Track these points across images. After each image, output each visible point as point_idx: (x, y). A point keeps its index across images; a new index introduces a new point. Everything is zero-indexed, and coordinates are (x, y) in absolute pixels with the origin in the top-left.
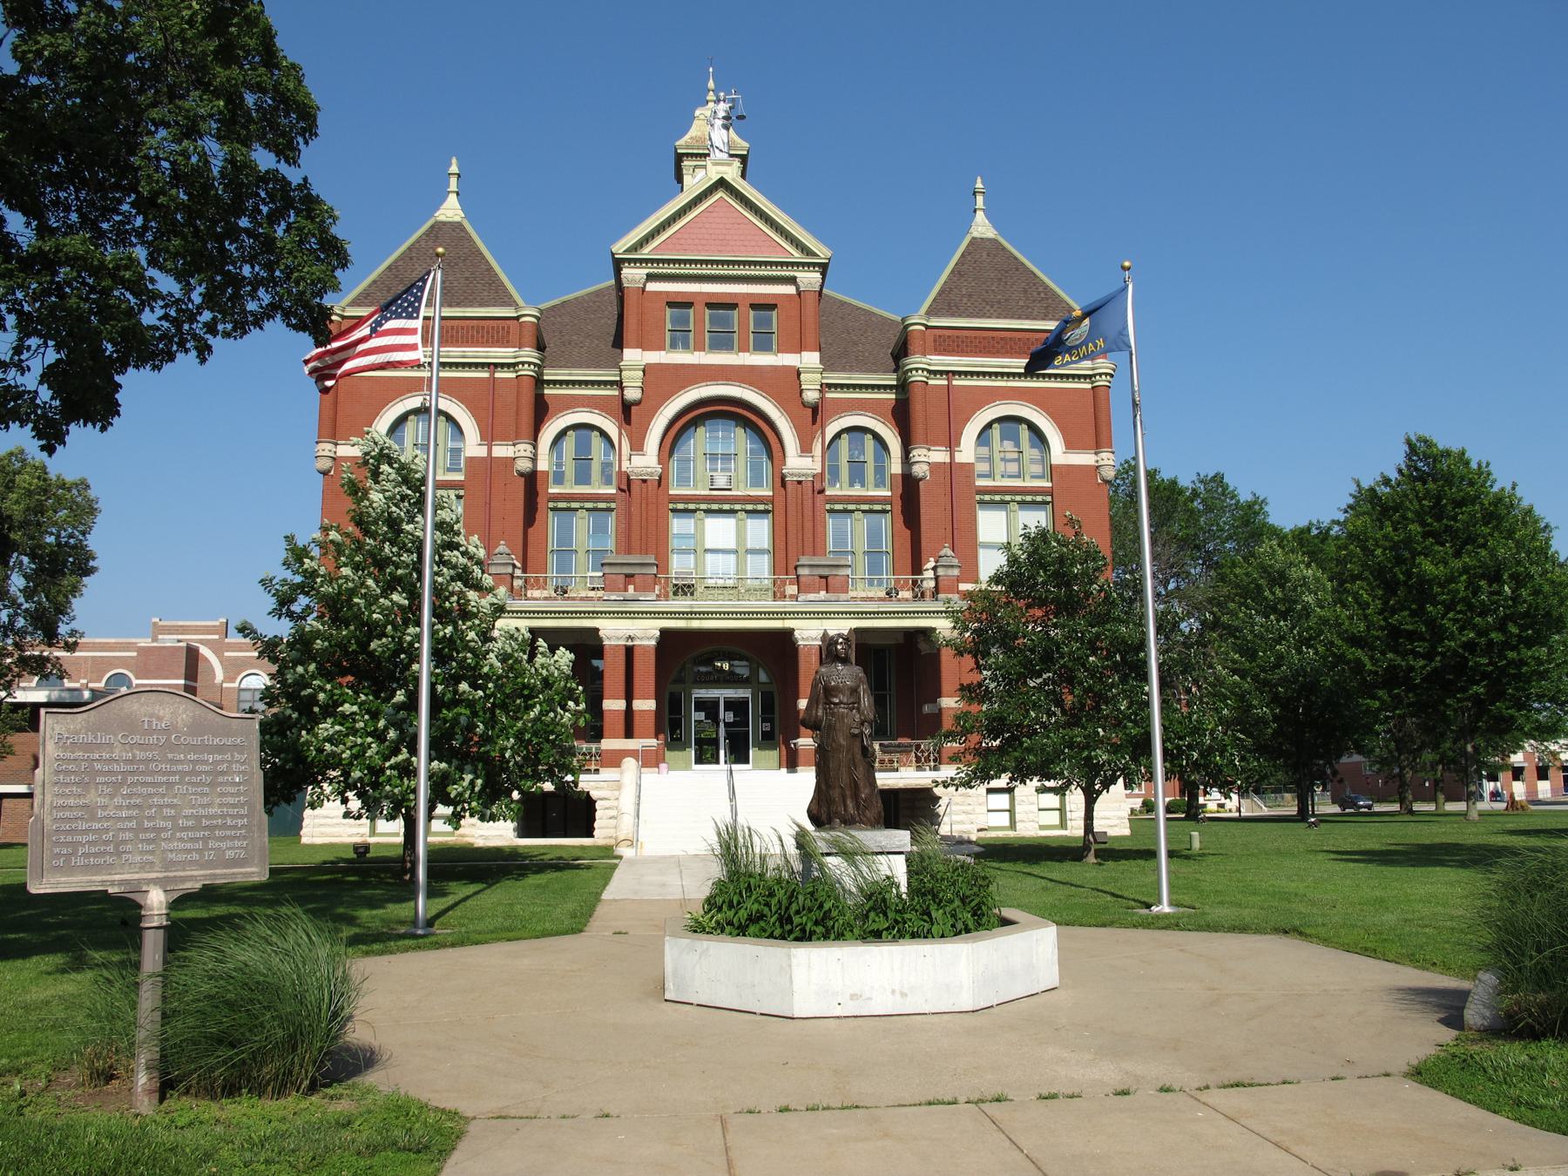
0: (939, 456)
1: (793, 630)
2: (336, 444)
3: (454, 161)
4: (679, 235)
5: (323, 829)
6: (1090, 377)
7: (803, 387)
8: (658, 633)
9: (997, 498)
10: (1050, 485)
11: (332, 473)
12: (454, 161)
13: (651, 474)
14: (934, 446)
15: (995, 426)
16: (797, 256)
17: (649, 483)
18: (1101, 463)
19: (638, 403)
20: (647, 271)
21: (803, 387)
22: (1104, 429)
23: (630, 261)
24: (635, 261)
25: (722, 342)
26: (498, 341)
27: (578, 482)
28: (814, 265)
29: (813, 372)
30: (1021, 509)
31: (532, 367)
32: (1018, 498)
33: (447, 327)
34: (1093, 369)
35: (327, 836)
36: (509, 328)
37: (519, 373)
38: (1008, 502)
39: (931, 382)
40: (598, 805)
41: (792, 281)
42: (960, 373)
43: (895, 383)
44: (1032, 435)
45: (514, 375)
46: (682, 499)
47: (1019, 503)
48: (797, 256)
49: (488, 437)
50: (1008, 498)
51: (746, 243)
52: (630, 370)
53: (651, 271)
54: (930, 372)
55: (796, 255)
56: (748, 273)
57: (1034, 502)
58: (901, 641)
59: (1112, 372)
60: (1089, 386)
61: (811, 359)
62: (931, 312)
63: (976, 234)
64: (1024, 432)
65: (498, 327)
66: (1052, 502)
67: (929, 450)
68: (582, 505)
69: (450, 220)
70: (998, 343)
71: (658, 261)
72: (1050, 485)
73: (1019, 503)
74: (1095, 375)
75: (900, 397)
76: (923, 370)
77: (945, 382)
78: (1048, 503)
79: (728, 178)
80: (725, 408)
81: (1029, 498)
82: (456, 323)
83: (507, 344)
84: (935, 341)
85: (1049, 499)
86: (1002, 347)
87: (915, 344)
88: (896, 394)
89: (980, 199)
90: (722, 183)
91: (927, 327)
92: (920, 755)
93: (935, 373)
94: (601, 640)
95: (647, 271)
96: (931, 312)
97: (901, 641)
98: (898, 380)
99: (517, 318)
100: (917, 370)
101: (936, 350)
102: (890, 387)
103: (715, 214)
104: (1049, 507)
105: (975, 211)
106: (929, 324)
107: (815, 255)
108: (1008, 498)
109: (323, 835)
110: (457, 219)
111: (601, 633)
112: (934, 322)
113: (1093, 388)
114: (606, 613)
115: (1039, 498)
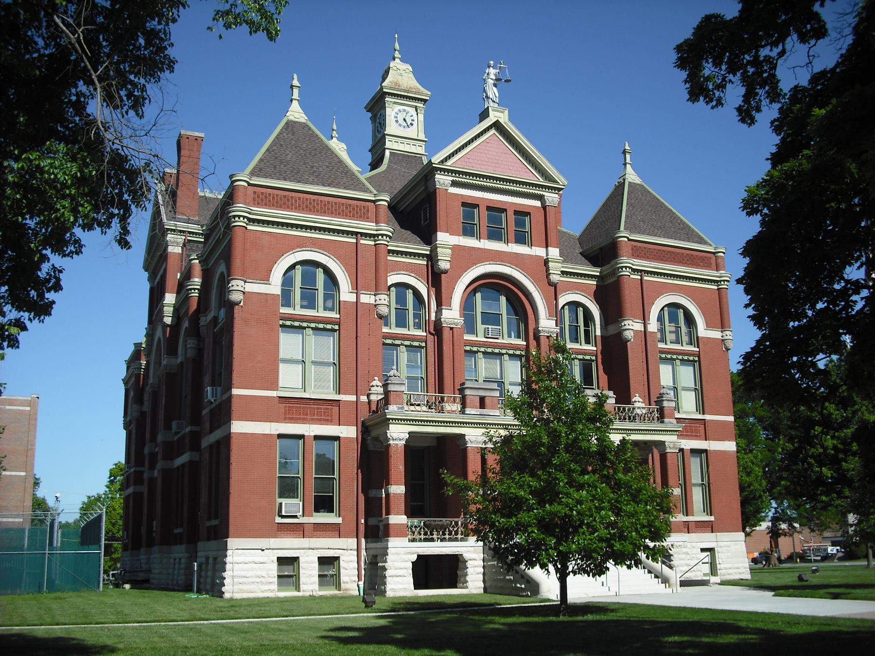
0: (639, 327)
1: (464, 435)
2: (245, 282)
3: (295, 76)
4: (468, 156)
5: (241, 586)
6: (717, 281)
7: (551, 271)
8: (408, 436)
9: (669, 356)
10: (338, 316)
11: (242, 304)
12: (295, 76)
13: (456, 324)
14: (635, 319)
15: (298, 267)
16: (541, 181)
17: (454, 330)
18: (726, 338)
19: (446, 272)
20: (451, 178)
21: (551, 271)
22: (725, 316)
23: (441, 170)
24: (445, 170)
25: (495, 235)
26: (361, 217)
27: (398, 325)
28: (555, 189)
29: (556, 262)
30: (681, 364)
31: (246, 220)
32: (313, 325)
33: (274, 194)
34: (720, 277)
35: (245, 592)
36: (368, 207)
37: (377, 242)
38: (305, 328)
39: (249, 227)
40: (469, 564)
41: (541, 198)
42: (648, 272)
43: (598, 274)
44: (328, 279)
45: (716, 288)
46: (391, 337)
47: (313, 329)
48: (541, 181)
49: (356, 287)
50: (305, 324)
51: (511, 168)
52: (443, 248)
53: (454, 179)
54: (250, 220)
55: (541, 180)
56: (515, 189)
57: (325, 329)
58: (434, 444)
59: (391, 235)
60: (716, 288)
61: (554, 252)
62: (253, 174)
63: (292, 118)
64: (320, 275)
65: (311, 199)
66: (339, 330)
67: (245, 282)
68: (309, 324)
69: (297, 120)
70: (667, 254)
71: (460, 173)
72: (338, 316)
73: (313, 329)
74: (720, 281)
75: (599, 284)
76: (244, 217)
77: (354, 241)
78: (336, 330)
79: (502, 121)
80: (502, 282)
81: (321, 326)
82: (331, 199)
83: (367, 219)
84: (632, 249)
85: (337, 327)
86: (669, 258)
87: (239, 195)
88: (597, 281)
89: (296, 92)
90: (497, 125)
91: (249, 184)
92: (451, 529)
93: (634, 270)
94: (388, 439)
95: (451, 178)
96: (253, 174)
97: (434, 444)
98: (600, 272)
99: (374, 202)
100: (239, 217)
101: (633, 255)
102: (423, 255)
103: (489, 145)
104: (336, 334)
105: (291, 101)
106: (251, 182)
107: (555, 182)
108: (305, 324)
109: (241, 591)
110: (305, 121)
111: (467, 438)
112: (255, 181)
113: (718, 289)
114: (469, 423)
115: (329, 327)
